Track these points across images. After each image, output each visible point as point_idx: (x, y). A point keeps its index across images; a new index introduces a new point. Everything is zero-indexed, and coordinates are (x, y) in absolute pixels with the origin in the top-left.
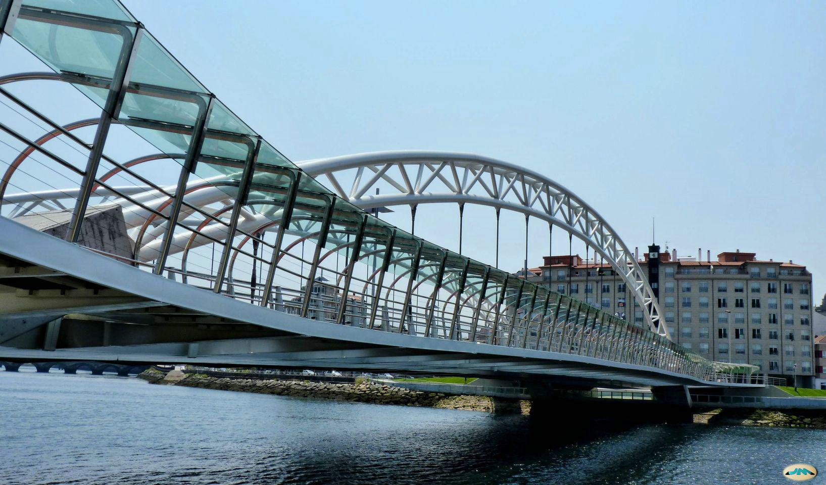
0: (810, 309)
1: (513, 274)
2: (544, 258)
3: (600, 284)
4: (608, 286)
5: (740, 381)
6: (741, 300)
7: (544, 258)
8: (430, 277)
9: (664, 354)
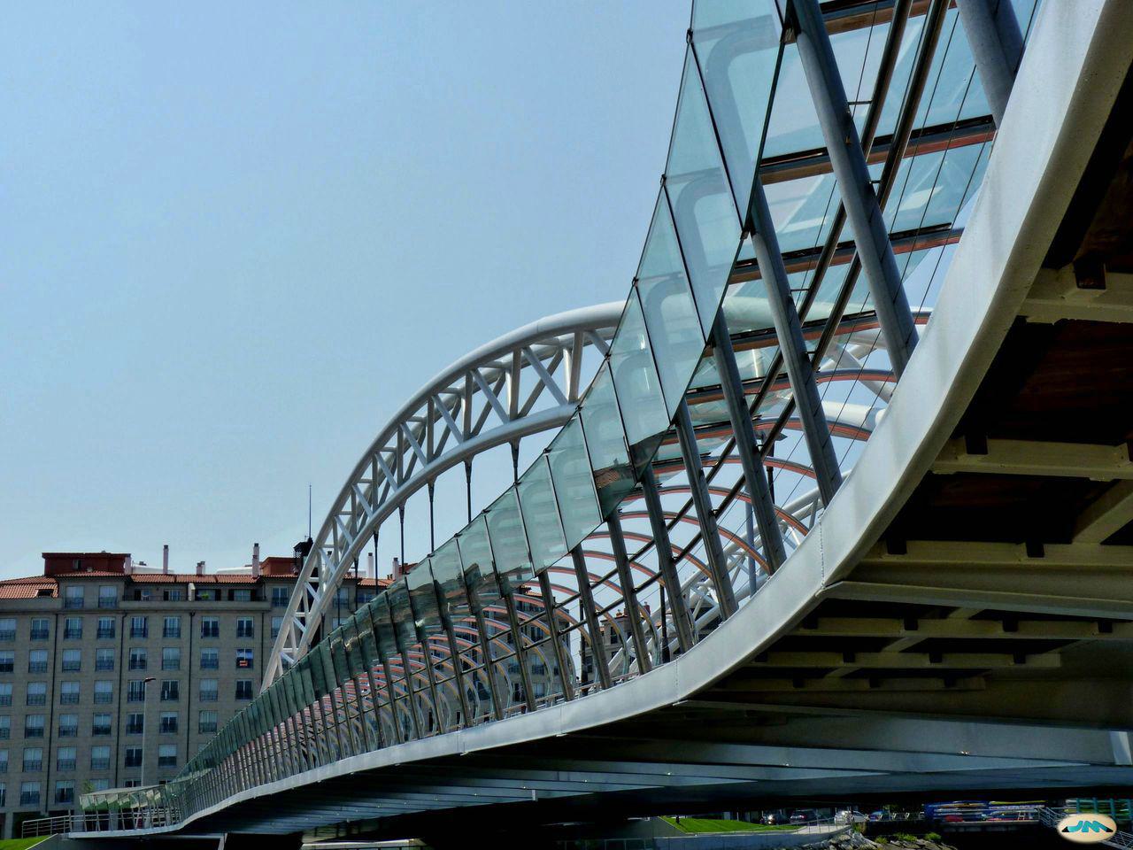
0: (619, 641)
2: (46, 556)
3: (197, 618)
4: (249, 623)
5: (130, 826)
6: (175, 684)
7: (46, 556)
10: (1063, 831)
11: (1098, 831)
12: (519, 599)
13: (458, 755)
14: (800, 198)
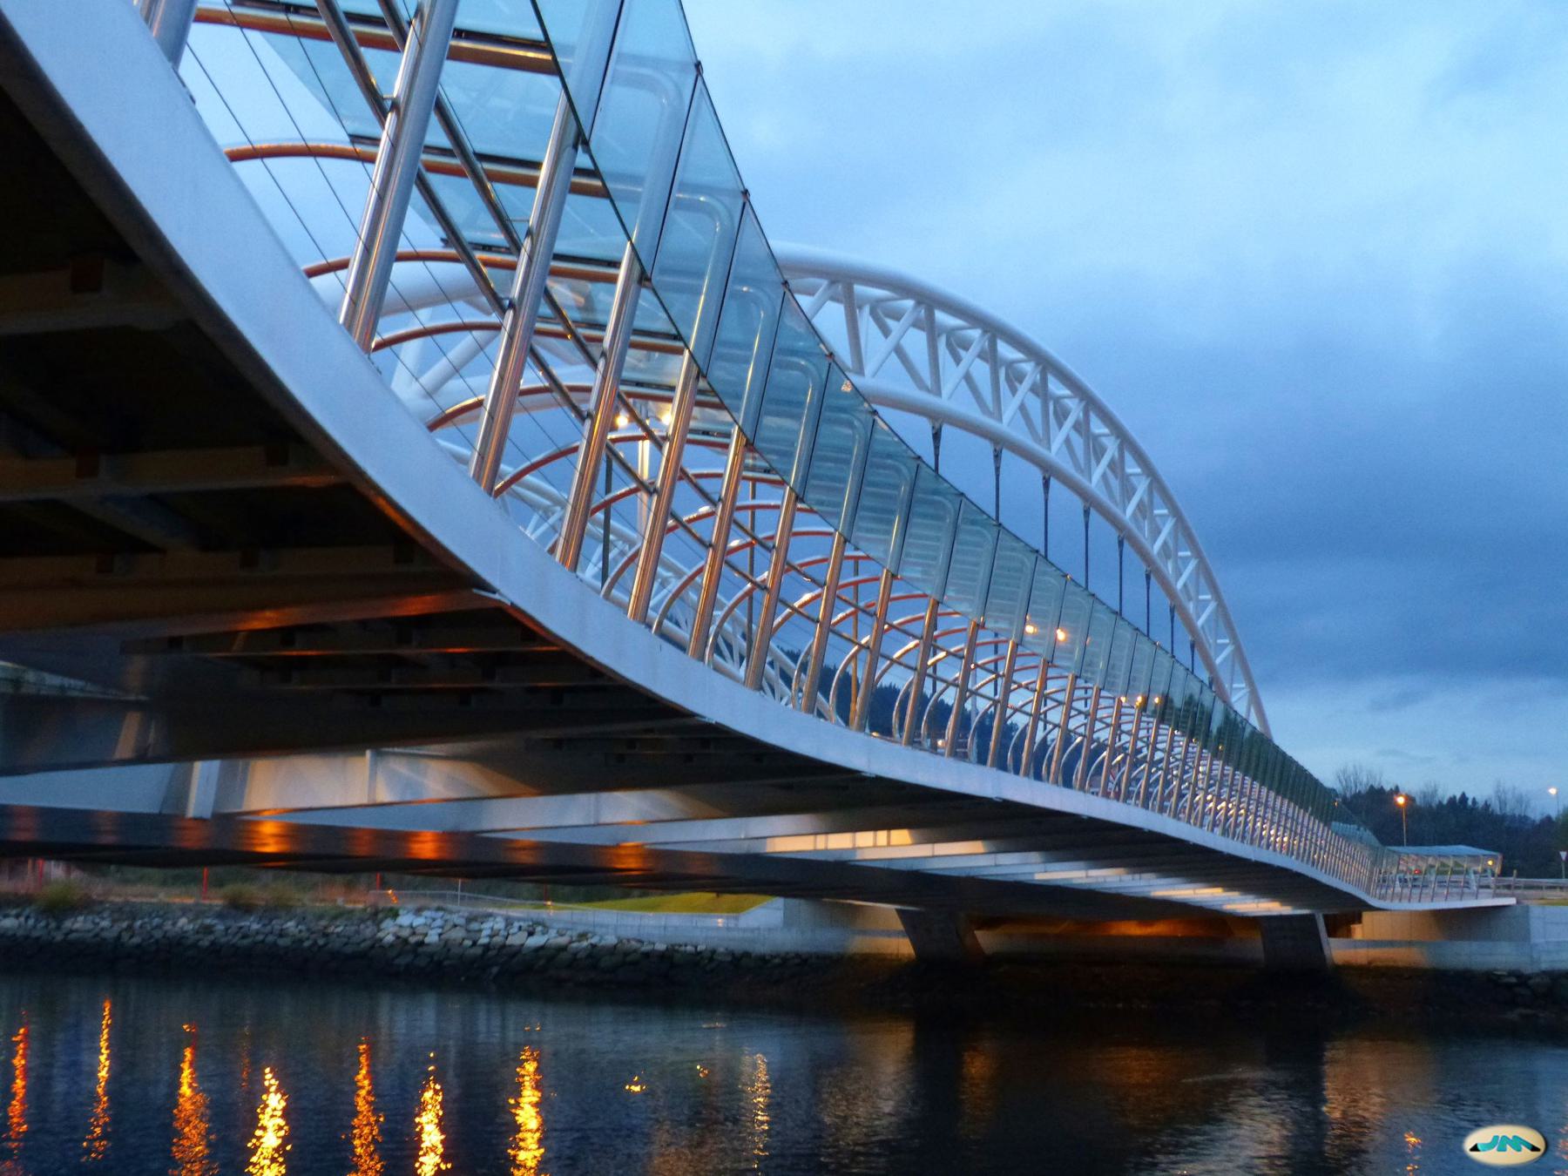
1: (1236, 712)
8: (1016, 710)
9: (1249, 804)
10: (1472, 1150)
11: (1519, 1150)
12: (1522, 1152)
13: (719, 893)
14: (557, 646)
